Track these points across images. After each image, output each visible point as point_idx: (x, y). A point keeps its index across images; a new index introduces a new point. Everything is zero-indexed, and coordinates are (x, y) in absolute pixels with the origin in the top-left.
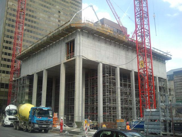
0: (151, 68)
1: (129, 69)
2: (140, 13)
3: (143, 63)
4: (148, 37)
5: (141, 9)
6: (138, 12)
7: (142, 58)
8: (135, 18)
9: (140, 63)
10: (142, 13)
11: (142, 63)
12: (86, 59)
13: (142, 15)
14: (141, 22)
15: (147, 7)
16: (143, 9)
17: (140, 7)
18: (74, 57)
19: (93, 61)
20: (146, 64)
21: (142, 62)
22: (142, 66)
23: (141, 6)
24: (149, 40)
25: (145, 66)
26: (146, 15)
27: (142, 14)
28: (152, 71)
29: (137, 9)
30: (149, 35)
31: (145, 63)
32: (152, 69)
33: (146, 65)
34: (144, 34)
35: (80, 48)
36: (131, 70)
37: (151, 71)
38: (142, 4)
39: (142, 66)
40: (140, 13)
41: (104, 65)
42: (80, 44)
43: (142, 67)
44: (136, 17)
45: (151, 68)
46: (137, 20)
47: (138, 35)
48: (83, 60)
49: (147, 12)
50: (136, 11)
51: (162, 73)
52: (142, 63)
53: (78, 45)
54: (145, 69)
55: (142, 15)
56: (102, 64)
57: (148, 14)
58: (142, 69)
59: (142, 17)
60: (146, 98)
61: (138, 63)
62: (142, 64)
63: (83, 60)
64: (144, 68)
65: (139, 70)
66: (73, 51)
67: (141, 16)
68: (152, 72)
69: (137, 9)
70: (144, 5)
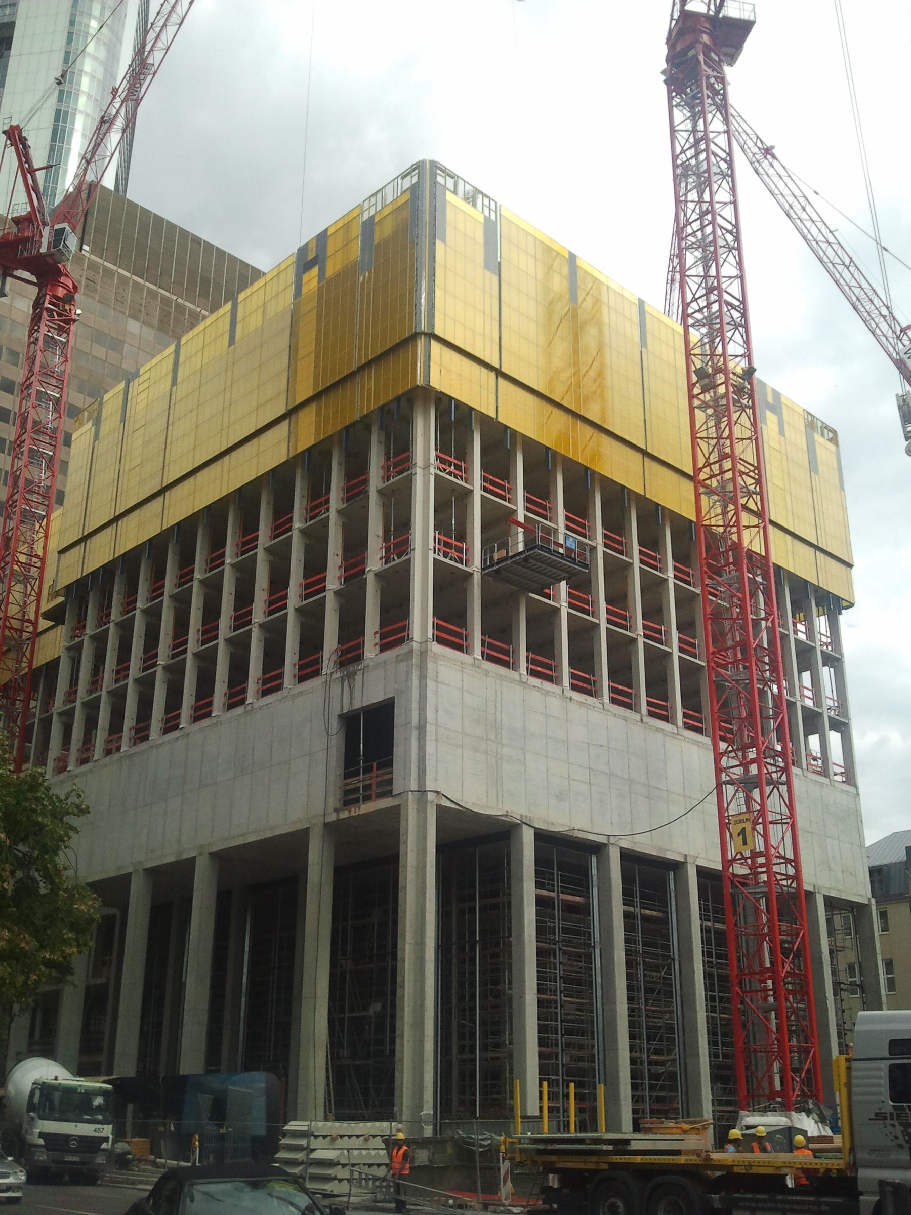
0: (790, 855)
1: (670, 855)
2: (709, 305)
3: (748, 826)
4: (783, 789)
5: (728, 450)
6: (709, 465)
7: (742, 801)
8: (692, 409)
9: (735, 829)
10: (733, 469)
11: (744, 829)
12: (453, 806)
13: (734, 479)
14: (717, 425)
15: (756, 440)
16: (739, 447)
17: (706, 276)
18: (389, 794)
19: (489, 816)
20: (765, 829)
21: (741, 821)
22: (745, 843)
23: (706, 197)
24: (785, 811)
25: (760, 846)
26: (750, 481)
27: (715, 307)
28: (797, 868)
29: (694, 289)
30: (784, 778)
31: (760, 828)
32: (795, 862)
33: (766, 836)
34: (769, 872)
35: (422, 748)
36: (680, 859)
37: (791, 871)
38: (723, 340)
39: (745, 843)
40: (702, 229)
41: (542, 837)
42: (422, 728)
43: (742, 848)
44: (696, 403)
45: (790, 855)
46: (700, 416)
47: (691, 321)
48: (440, 809)
49: (743, 302)
50: (678, 150)
51: (843, 872)
52: (744, 829)
53: (415, 734)
54: (761, 860)
55: (734, 479)
56: (532, 831)
57: (759, 474)
58: (743, 858)
59: (730, 487)
60: (768, 1019)
61: (724, 826)
62: (743, 831)
63: (440, 809)
64: (755, 854)
65: (727, 863)
66: (387, 763)
67: (723, 487)
68: (797, 877)
69: (694, 289)
70: (728, 269)
